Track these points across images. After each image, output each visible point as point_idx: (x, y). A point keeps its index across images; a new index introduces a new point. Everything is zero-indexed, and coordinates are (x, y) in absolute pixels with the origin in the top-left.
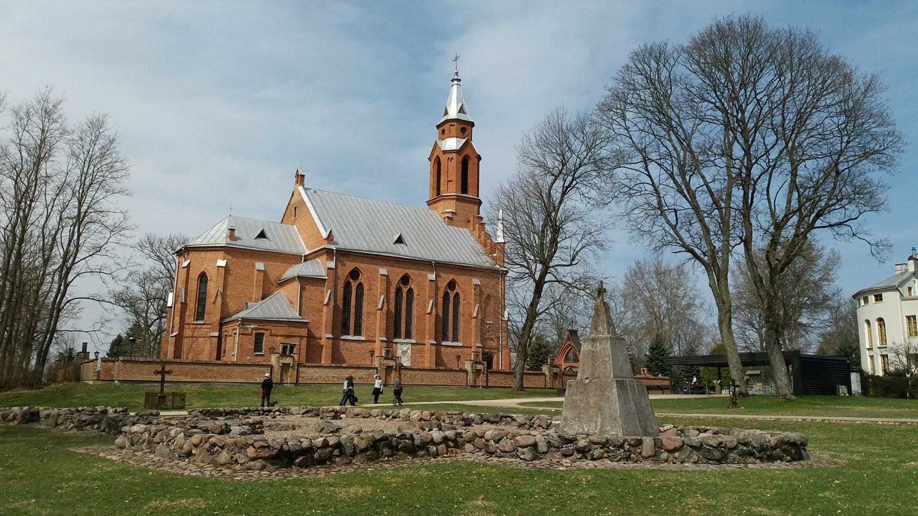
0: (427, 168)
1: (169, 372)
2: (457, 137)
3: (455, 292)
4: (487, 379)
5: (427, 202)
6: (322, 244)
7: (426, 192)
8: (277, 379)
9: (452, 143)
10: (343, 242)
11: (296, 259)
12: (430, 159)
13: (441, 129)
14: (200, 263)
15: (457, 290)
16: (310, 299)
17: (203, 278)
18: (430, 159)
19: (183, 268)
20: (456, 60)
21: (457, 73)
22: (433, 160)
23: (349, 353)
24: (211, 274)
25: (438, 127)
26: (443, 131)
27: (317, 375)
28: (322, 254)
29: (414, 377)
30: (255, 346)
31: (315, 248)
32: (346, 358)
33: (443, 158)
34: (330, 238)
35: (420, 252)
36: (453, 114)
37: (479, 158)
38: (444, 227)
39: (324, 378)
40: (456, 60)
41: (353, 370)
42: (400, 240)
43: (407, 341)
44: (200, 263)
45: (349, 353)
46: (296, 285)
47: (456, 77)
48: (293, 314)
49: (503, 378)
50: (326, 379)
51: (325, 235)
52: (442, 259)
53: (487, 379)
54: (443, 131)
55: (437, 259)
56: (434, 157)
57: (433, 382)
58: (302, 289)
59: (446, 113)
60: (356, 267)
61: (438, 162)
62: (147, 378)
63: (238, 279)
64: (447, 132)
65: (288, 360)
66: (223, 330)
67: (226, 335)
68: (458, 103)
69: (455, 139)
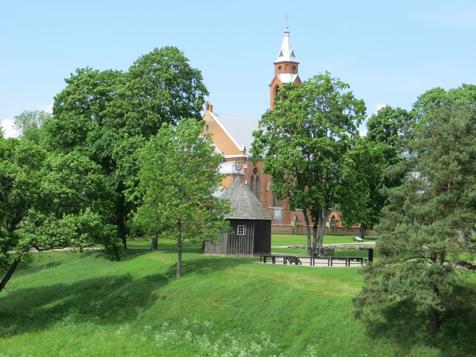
13: (278, 65)
20: (287, 17)
21: (287, 27)
36: (287, 58)
40: (287, 17)
47: (287, 31)
51: (242, 150)
54: (280, 67)
56: (274, 85)
64: (283, 68)
68: (290, 49)
69: (289, 74)
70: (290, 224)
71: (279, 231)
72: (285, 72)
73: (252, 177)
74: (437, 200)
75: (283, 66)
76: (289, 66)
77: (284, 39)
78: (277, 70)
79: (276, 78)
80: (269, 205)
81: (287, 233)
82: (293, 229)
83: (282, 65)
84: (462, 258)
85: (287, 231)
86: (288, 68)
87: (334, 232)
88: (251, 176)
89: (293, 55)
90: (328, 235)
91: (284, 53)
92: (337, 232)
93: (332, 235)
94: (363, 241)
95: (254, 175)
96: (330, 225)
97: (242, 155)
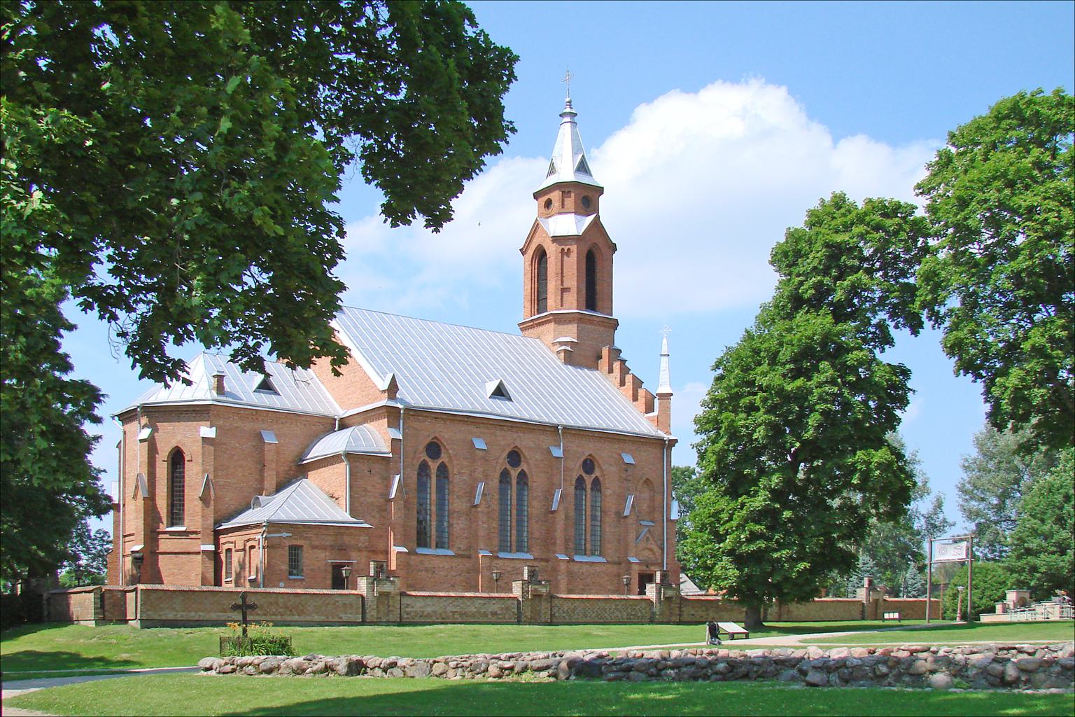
0: (521, 266)
1: (253, 607)
2: (576, 213)
3: (593, 476)
4: (681, 611)
5: (519, 325)
6: (376, 399)
7: (521, 310)
8: (372, 616)
9: (568, 224)
10: (410, 396)
11: (332, 425)
12: (523, 251)
13: (545, 198)
14: (172, 435)
15: (444, 458)
16: (365, 490)
17: (177, 458)
18: (523, 251)
19: (141, 441)
21: (570, 102)
22: (530, 252)
23: (430, 575)
24: (192, 451)
25: (537, 196)
26: (548, 204)
27: (429, 609)
28: (379, 418)
29: (574, 611)
30: (291, 566)
31: (359, 405)
32: (165, 580)
33: (552, 250)
34: (393, 389)
35: (450, 399)
36: (567, 173)
37: (613, 248)
38: (560, 368)
39: (440, 614)
41: (480, 601)
42: (500, 392)
43: (441, 552)
44: (172, 435)
45: (430, 575)
46: (342, 469)
47: (568, 110)
48: (339, 514)
49: (704, 608)
50: (443, 615)
51: (384, 385)
52: (572, 423)
53: (681, 611)
54: (548, 204)
55: (564, 423)
57: (602, 618)
58: (353, 475)
59: (552, 170)
60: (436, 438)
61: (541, 255)
62: (182, 616)
63: (235, 458)
64: (556, 204)
65: (387, 588)
66: (222, 541)
67: (229, 550)
68: (575, 153)
69: (572, 216)
70: (511, 590)
71: (461, 614)
72: (562, 211)
73: (424, 468)
74: (894, 676)
75: (556, 196)
76: (573, 195)
77: (561, 131)
78: (543, 210)
79: (536, 226)
80: (482, 545)
81: (494, 619)
82: (519, 608)
83: (551, 196)
84: (265, 519)
85: (493, 614)
86: (570, 202)
87: (671, 614)
88: (417, 464)
89: (583, 167)
90: (652, 622)
91: (557, 165)
92: (685, 614)
93: (668, 623)
94: (747, 637)
95: (428, 459)
96: (659, 593)
97: (384, 402)
